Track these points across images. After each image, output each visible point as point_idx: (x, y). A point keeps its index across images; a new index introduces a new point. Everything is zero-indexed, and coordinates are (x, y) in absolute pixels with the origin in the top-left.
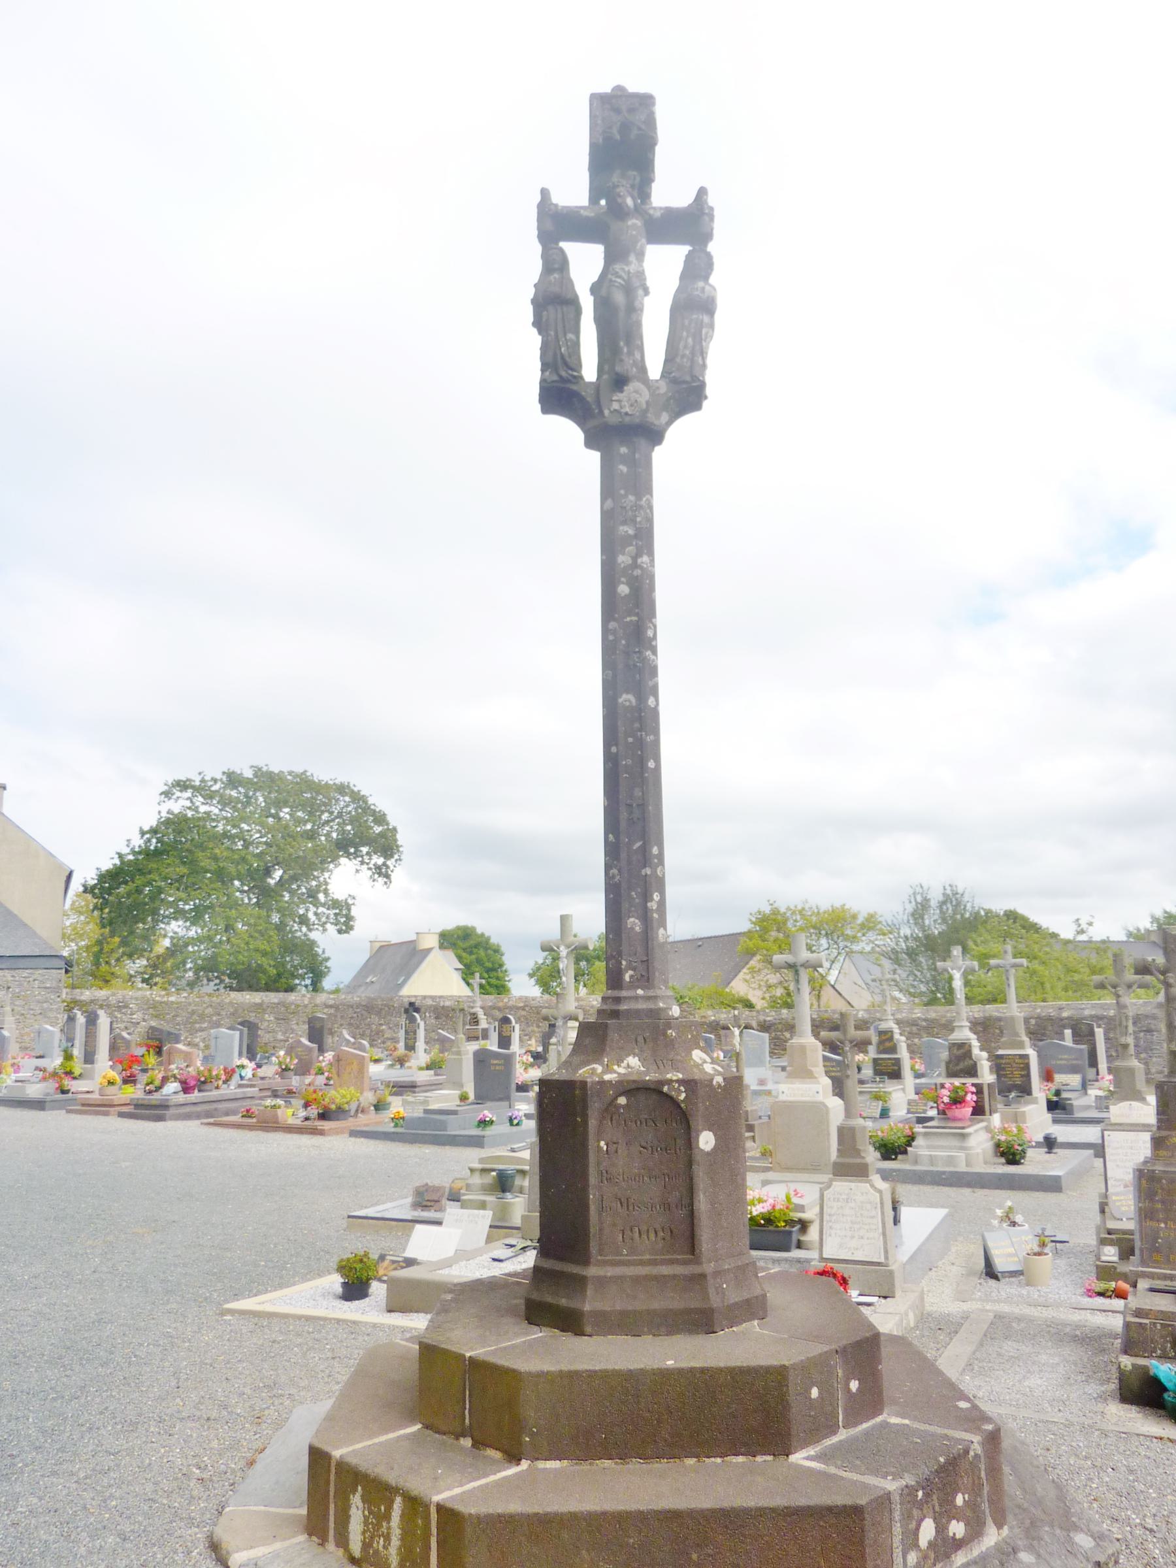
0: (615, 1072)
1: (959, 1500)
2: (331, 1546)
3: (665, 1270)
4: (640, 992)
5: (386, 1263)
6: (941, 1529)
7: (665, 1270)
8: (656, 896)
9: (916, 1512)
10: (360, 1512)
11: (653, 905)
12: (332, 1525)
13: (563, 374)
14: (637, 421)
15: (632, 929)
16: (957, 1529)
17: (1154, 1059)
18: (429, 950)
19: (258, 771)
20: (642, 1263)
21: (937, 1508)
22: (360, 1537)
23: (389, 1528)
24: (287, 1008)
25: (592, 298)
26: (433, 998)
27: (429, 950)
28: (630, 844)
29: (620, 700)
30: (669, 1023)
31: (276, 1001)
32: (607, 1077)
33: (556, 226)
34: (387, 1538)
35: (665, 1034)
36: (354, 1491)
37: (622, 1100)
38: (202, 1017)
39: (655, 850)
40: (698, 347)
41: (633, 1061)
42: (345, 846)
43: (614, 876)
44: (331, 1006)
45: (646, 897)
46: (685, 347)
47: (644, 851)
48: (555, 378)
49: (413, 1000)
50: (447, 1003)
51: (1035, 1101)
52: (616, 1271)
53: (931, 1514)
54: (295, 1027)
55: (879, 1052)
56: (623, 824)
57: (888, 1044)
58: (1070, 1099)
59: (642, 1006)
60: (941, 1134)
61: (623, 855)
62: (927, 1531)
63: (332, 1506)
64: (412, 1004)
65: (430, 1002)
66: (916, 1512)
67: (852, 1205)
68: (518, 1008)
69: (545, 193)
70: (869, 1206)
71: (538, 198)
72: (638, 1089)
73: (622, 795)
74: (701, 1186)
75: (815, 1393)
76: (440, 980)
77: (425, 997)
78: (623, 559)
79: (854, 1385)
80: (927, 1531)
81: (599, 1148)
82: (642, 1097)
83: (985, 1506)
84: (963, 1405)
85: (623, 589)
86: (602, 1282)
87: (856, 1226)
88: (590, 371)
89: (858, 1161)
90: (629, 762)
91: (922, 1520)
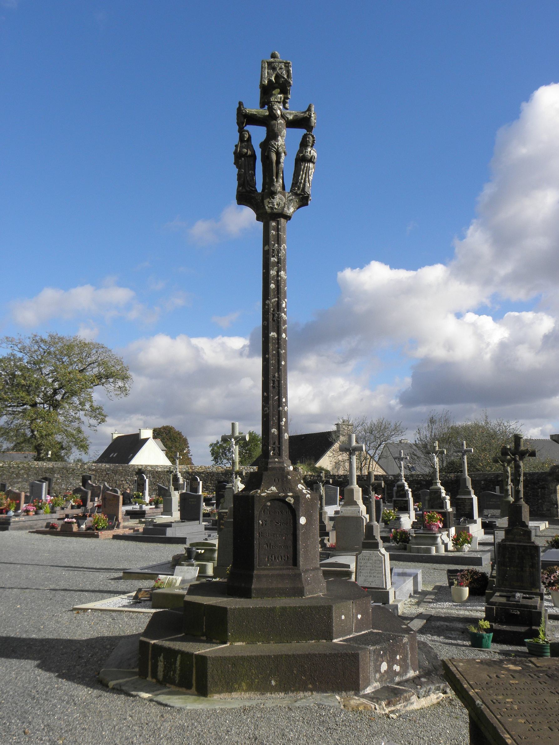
0: (266, 492)
1: (398, 657)
2: (149, 679)
3: (285, 572)
4: (276, 460)
5: (142, 592)
6: (390, 667)
7: (285, 572)
8: (284, 419)
9: (380, 659)
10: (162, 663)
11: (283, 423)
12: (150, 670)
13: (248, 189)
14: (280, 211)
15: (274, 433)
16: (397, 668)
17: (546, 503)
18: (146, 440)
19: (51, 336)
20: (275, 569)
21: (389, 659)
22: (162, 673)
23: (175, 667)
24: (67, 471)
25: (261, 150)
26: (151, 466)
27: (146, 440)
28: (273, 397)
29: (270, 335)
30: (288, 473)
31: (61, 466)
32: (263, 494)
33: (245, 119)
34: (175, 672)
35: (287, 477)
36: (160, 656)
37: (269, 504)
38: (18, 475)
39: (284, 400)
40: (307, 179)
41: (274, 488)
42: (101, 378)
43: (266, 411)
44: (93, 470)
45: (280, 420)
46: (302, 179)
47: (279, 400)
48: (244, 190)
49: (140, 467)
50: (160, 470)
51: (475, 522)
52: (264, 574)
53: (386, 660)
54: (71, 481)
55: (397, 497)
56: (271, 389)
57: (401, 493)
58: (495, 522)
59: (277, 465)
60: (421, 536)
61: (271, 402)
62: (384, 667)
63: (150, 663)
64: (140, 470)
65: (149, 468)
66: (380, 659)
67: (371, 561)
68: (200, 473)
69: (240, 104)
70: (378, 562)
71: (238, 106)
72: (275, 499)
73: (271, 376)
74: (300, 538)
75: (343, 617)
76: (152, 455)
77: (146, 466)
78: (273, 273)
79: (359, 616)
80: (384, 667)
81: (259, 523)
82: (276, 502)
83: (409, 661)
84: (404, 626)
85: (273, 286)
86: (259, 577)
87: (372, 571)
88: (259, 188)
89: (374, 541)
90: (274, 362)
91: (383, 662)
